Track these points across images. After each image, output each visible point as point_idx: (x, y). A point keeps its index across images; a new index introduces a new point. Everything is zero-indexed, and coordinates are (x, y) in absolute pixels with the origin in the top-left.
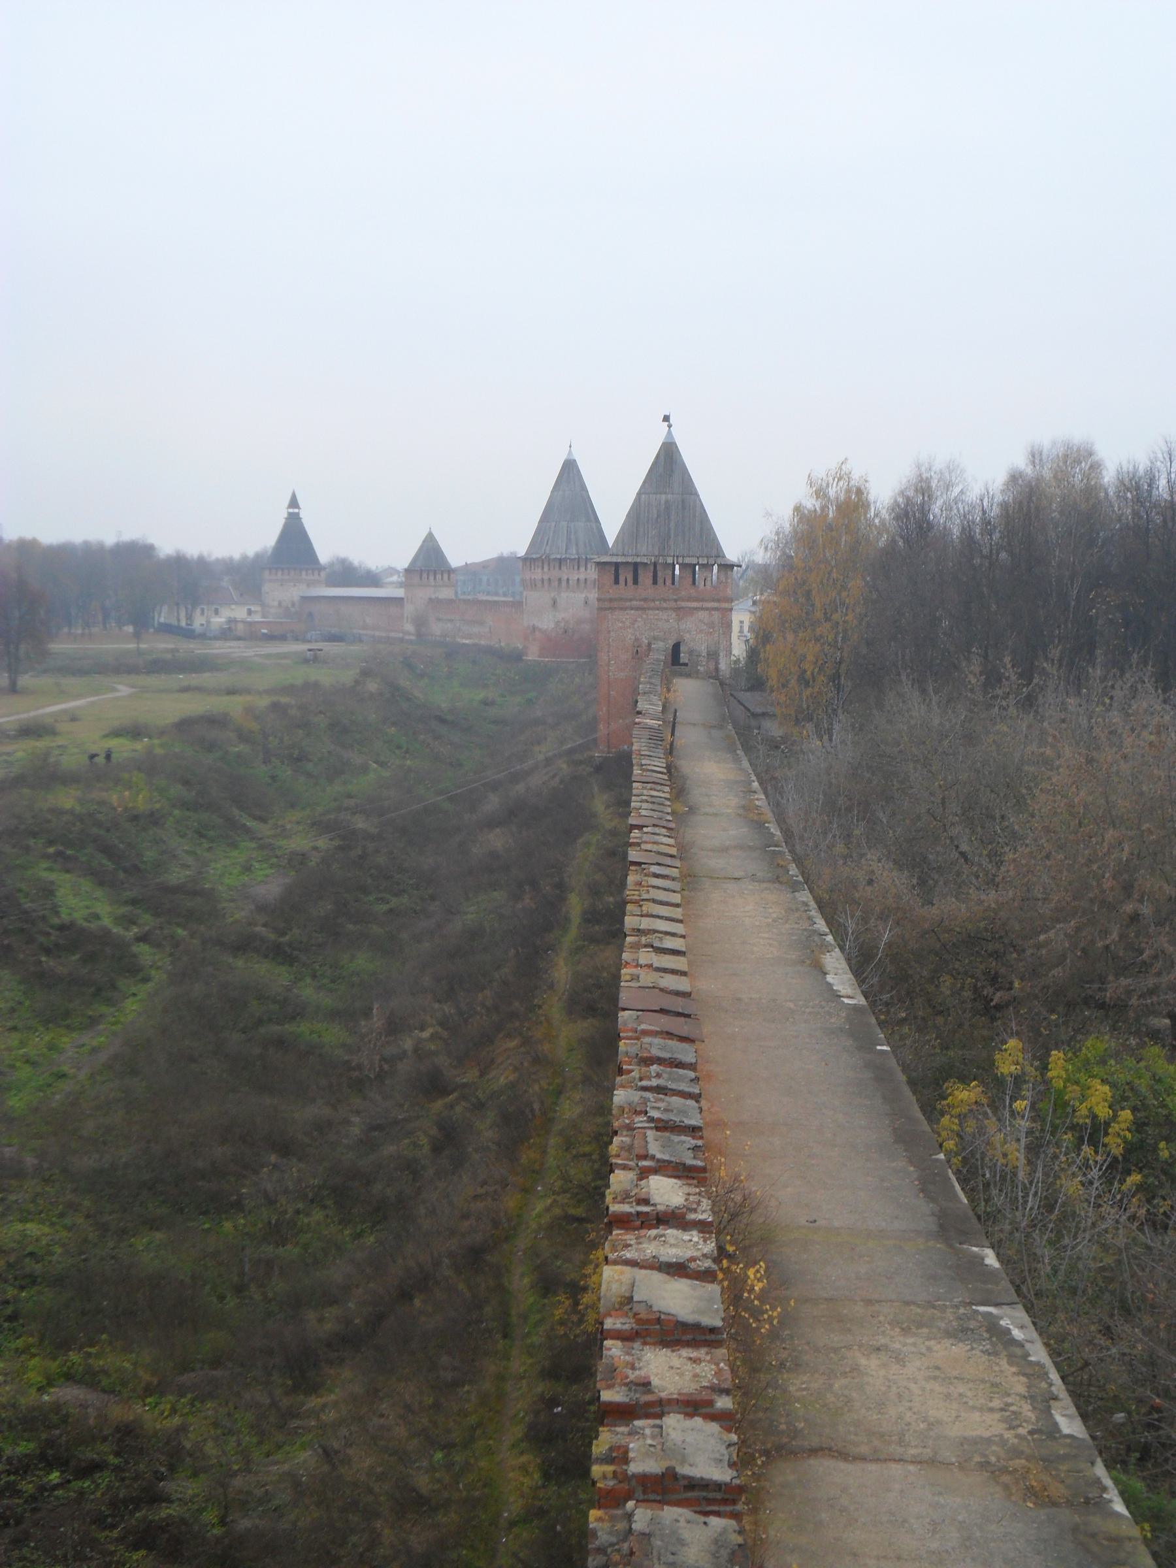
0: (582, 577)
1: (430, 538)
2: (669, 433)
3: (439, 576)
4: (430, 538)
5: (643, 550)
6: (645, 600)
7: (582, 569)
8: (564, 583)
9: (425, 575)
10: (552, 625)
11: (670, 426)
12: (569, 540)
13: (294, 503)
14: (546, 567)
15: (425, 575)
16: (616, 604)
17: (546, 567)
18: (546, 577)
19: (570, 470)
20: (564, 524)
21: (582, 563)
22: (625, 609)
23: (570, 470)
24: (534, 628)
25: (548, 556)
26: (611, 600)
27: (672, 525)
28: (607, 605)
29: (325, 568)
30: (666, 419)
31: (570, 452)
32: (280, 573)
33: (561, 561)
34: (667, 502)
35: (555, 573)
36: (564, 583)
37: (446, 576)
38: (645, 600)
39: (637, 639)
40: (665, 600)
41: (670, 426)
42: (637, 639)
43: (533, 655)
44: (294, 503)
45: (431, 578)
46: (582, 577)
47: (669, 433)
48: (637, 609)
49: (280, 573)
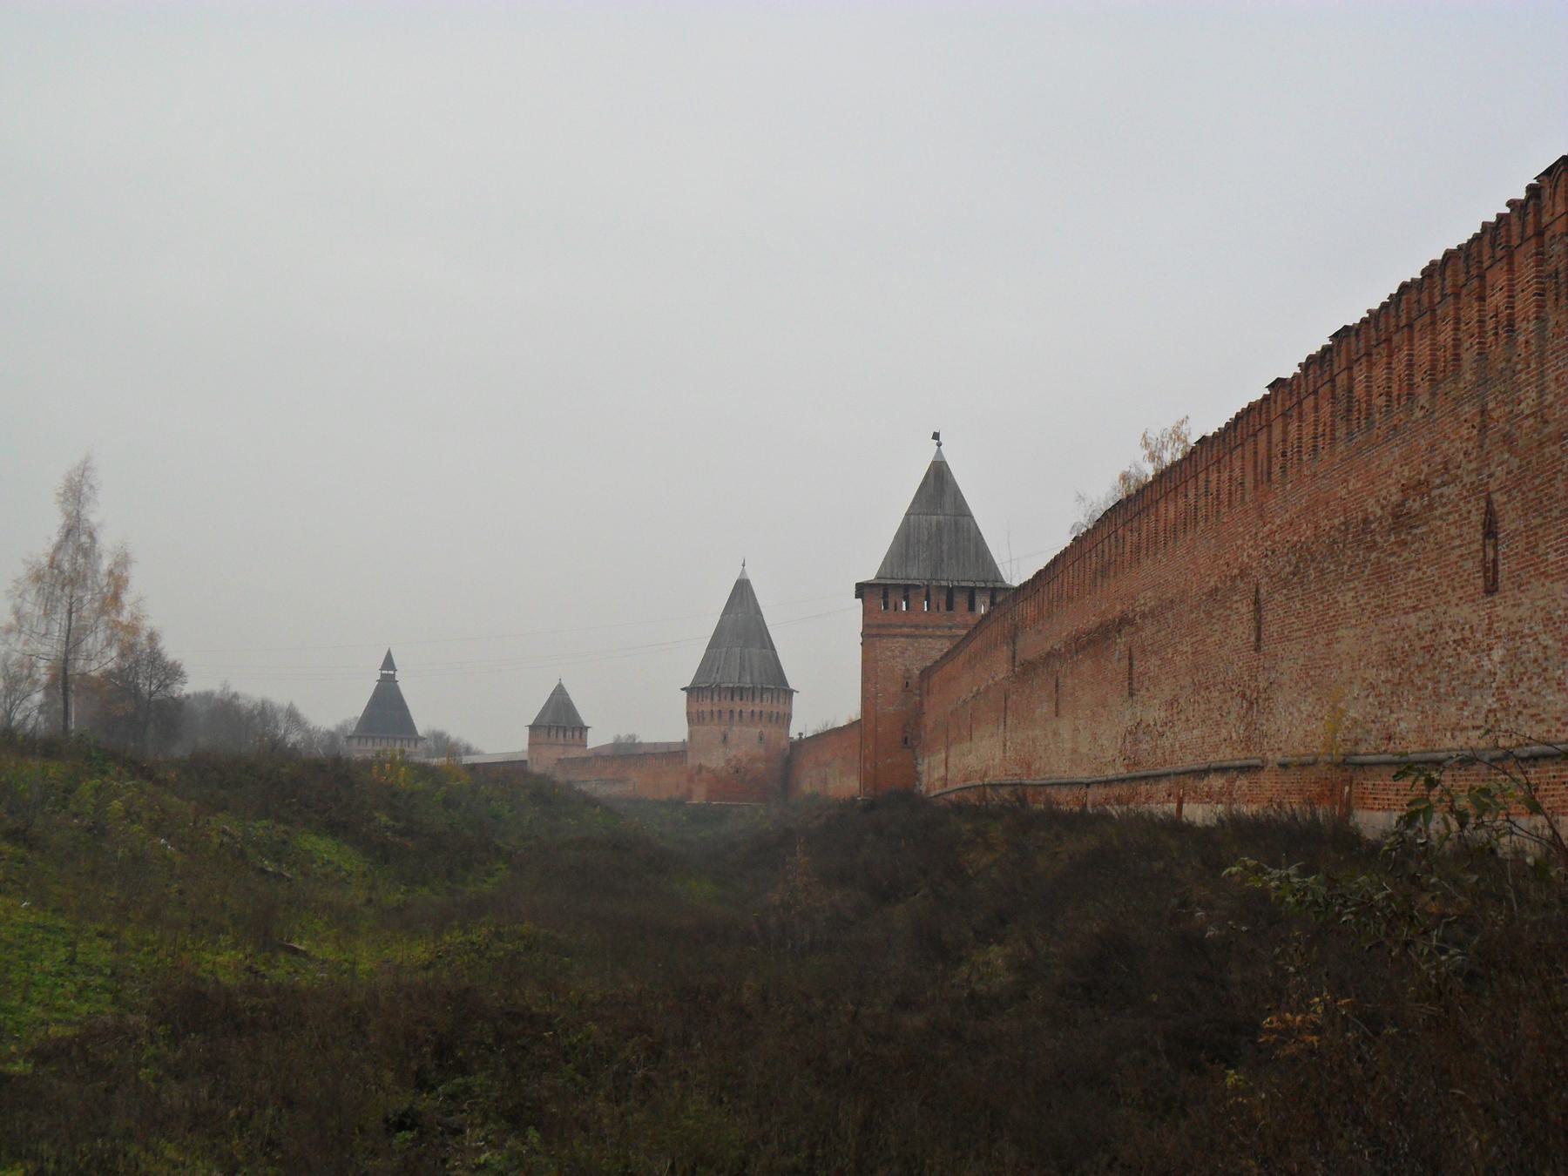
0: (757, 709)
1: (560, 691)
2: (939, 452)
3: (569, 734)
4: (560, 691)
5: (914, 574)
6: (917, 627)
7: (757, 701)
8: (736, 715)
9: (553, 732)
10: (722, 764)
11: (939, 445)
12: (742, 668)
13: (389, 663)
14: (716, 698)
15: (553, 732)
16: (885, 632)
17: (716, 698)
18: (715, 709)
19: (742, 591)
20: (737, 650)
21: (757, 694)
22: (895, 636)
23: (742, 591)
24: (701, 767)
25: (718, 686)
26: (878, 626)
27: (945, 547)
28: (874, 631)
29: (422, 739)
30: (936, 436)
31: (743, 572)
32: (370, 743)
33: (732, 691)
34: (938, 523)
35: (726, 704)
36: (736, 715)
37: (577, 734)
38: (917, 627)
39: (907, 670)
40: (938, 627)
41: (939, 445)
42: (907, 670)
43: (699, 798)
44: (389, 663)
45: (561, 735)
46: (757, 709)
47: (939, 452)
48: (907, 636)
49: (370, 743)
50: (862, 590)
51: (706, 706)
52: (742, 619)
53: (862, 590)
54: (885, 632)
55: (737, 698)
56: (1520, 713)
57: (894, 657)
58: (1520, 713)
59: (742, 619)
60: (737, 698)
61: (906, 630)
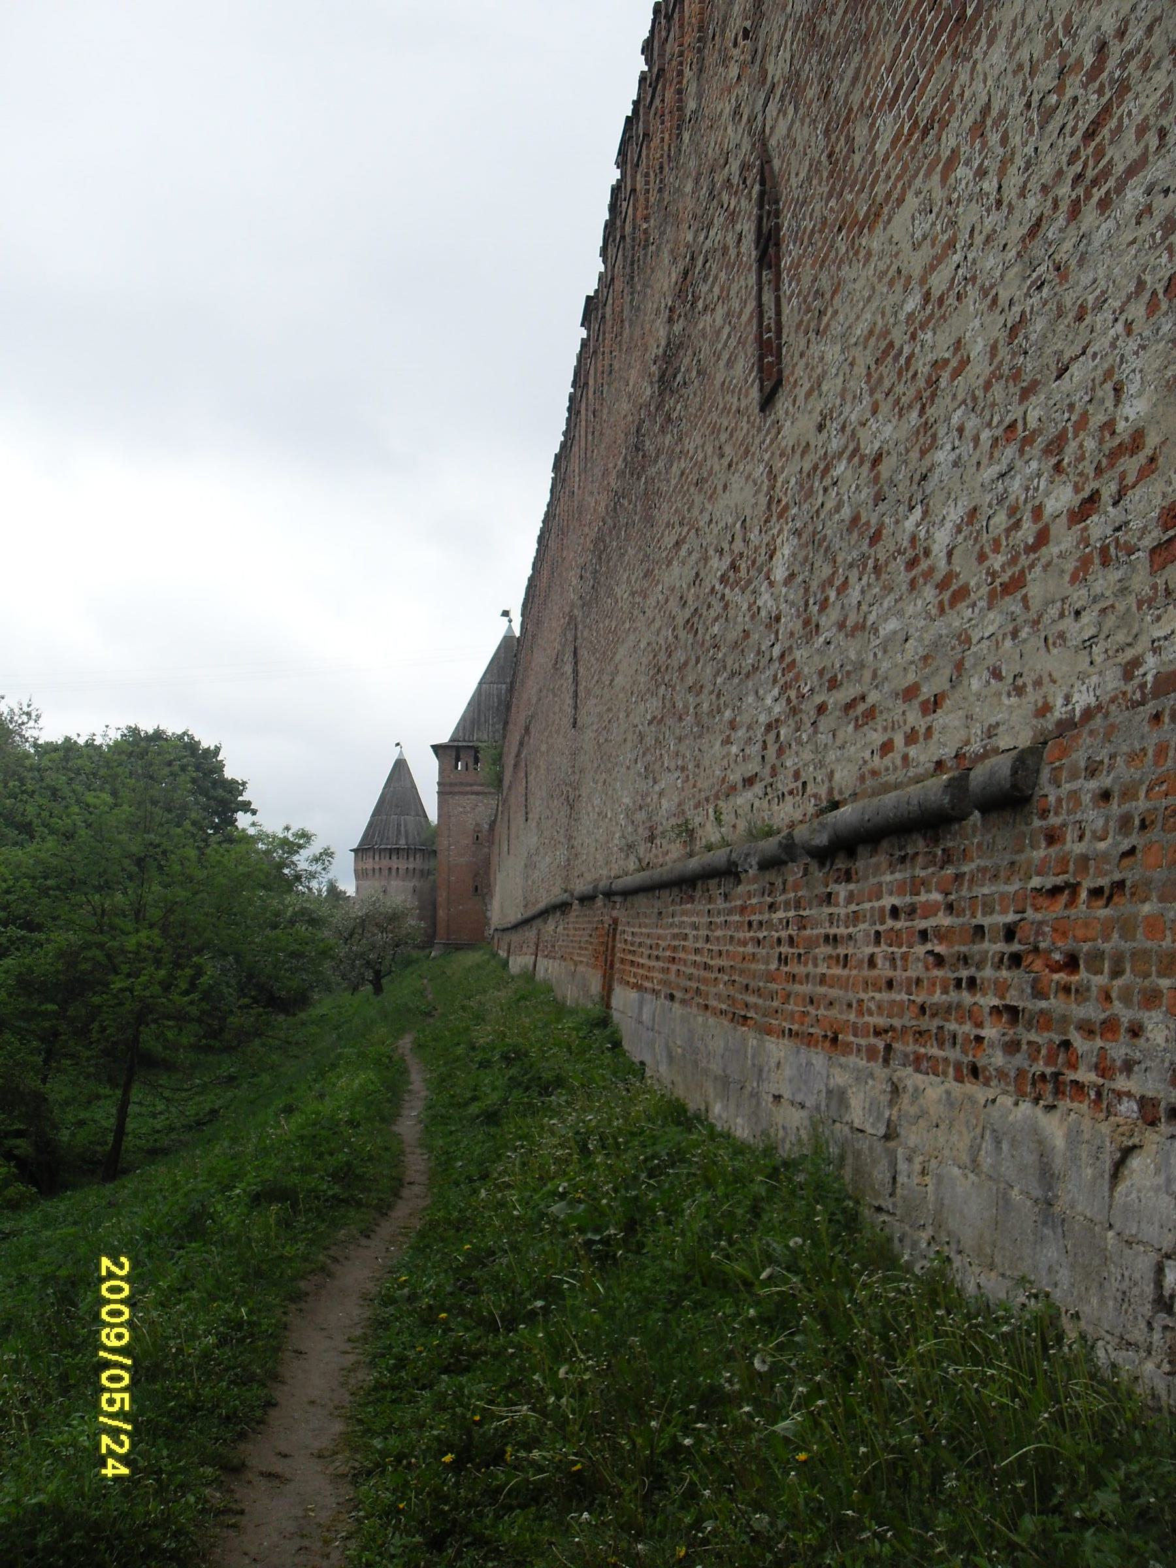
8: (394, 872)
16: (456, 789)
22: (467, 793)
28: (448, 789)
35: (385, 863)
36: (394, 872)
39: (477, 825)
42: (477, 825)
46: (411, 866)
48: (477, 793)
50: (437, 749)
51: (369, 864)
52: (400, 769)
53: (437, 749)
54: (456, 789)
55: (394, 857)
56: (821, 709)
57: (465, 813)
58: (821, 709)
59: (400, 769)
60: (394, 857)
61: (476, 788)
